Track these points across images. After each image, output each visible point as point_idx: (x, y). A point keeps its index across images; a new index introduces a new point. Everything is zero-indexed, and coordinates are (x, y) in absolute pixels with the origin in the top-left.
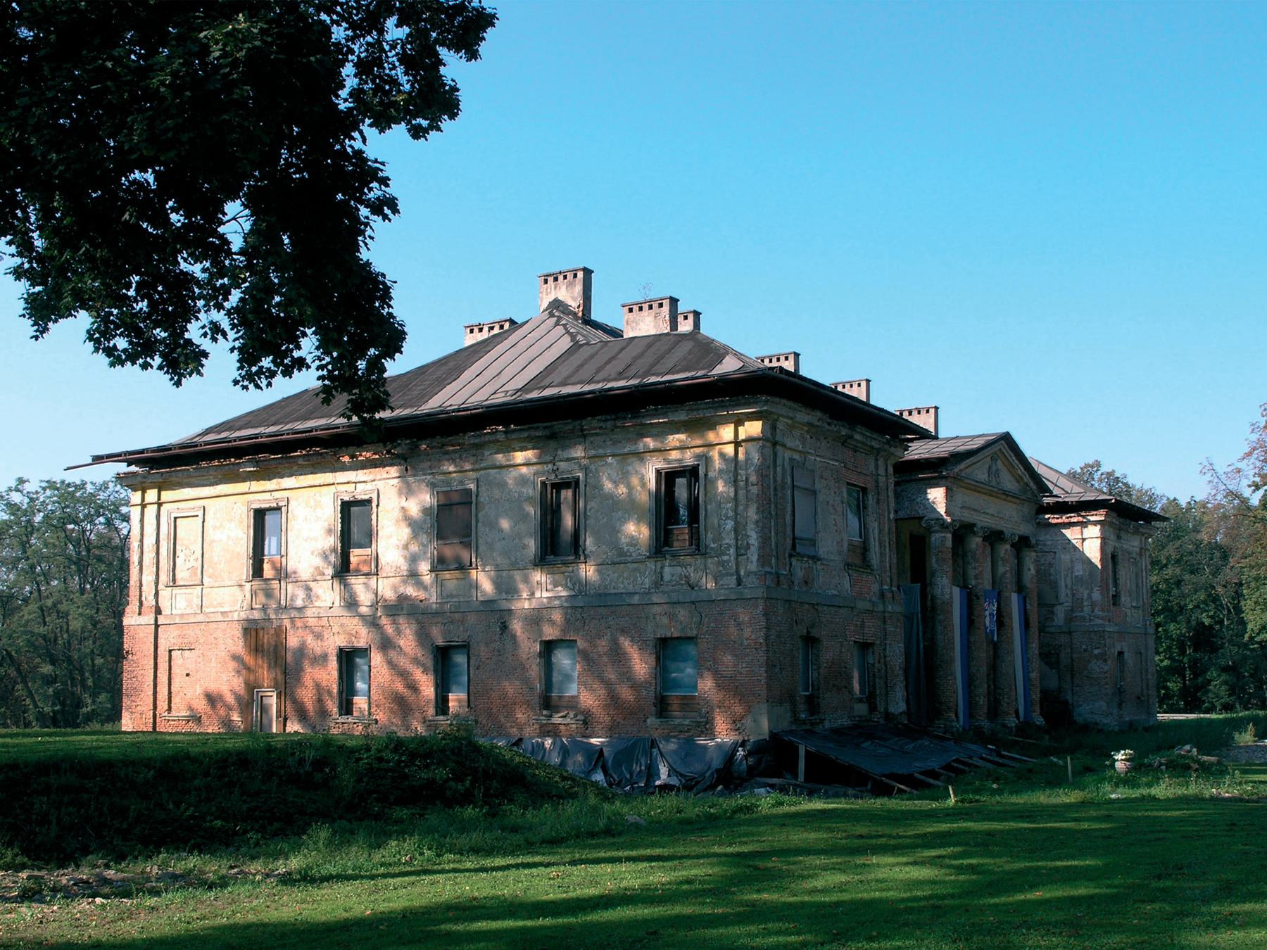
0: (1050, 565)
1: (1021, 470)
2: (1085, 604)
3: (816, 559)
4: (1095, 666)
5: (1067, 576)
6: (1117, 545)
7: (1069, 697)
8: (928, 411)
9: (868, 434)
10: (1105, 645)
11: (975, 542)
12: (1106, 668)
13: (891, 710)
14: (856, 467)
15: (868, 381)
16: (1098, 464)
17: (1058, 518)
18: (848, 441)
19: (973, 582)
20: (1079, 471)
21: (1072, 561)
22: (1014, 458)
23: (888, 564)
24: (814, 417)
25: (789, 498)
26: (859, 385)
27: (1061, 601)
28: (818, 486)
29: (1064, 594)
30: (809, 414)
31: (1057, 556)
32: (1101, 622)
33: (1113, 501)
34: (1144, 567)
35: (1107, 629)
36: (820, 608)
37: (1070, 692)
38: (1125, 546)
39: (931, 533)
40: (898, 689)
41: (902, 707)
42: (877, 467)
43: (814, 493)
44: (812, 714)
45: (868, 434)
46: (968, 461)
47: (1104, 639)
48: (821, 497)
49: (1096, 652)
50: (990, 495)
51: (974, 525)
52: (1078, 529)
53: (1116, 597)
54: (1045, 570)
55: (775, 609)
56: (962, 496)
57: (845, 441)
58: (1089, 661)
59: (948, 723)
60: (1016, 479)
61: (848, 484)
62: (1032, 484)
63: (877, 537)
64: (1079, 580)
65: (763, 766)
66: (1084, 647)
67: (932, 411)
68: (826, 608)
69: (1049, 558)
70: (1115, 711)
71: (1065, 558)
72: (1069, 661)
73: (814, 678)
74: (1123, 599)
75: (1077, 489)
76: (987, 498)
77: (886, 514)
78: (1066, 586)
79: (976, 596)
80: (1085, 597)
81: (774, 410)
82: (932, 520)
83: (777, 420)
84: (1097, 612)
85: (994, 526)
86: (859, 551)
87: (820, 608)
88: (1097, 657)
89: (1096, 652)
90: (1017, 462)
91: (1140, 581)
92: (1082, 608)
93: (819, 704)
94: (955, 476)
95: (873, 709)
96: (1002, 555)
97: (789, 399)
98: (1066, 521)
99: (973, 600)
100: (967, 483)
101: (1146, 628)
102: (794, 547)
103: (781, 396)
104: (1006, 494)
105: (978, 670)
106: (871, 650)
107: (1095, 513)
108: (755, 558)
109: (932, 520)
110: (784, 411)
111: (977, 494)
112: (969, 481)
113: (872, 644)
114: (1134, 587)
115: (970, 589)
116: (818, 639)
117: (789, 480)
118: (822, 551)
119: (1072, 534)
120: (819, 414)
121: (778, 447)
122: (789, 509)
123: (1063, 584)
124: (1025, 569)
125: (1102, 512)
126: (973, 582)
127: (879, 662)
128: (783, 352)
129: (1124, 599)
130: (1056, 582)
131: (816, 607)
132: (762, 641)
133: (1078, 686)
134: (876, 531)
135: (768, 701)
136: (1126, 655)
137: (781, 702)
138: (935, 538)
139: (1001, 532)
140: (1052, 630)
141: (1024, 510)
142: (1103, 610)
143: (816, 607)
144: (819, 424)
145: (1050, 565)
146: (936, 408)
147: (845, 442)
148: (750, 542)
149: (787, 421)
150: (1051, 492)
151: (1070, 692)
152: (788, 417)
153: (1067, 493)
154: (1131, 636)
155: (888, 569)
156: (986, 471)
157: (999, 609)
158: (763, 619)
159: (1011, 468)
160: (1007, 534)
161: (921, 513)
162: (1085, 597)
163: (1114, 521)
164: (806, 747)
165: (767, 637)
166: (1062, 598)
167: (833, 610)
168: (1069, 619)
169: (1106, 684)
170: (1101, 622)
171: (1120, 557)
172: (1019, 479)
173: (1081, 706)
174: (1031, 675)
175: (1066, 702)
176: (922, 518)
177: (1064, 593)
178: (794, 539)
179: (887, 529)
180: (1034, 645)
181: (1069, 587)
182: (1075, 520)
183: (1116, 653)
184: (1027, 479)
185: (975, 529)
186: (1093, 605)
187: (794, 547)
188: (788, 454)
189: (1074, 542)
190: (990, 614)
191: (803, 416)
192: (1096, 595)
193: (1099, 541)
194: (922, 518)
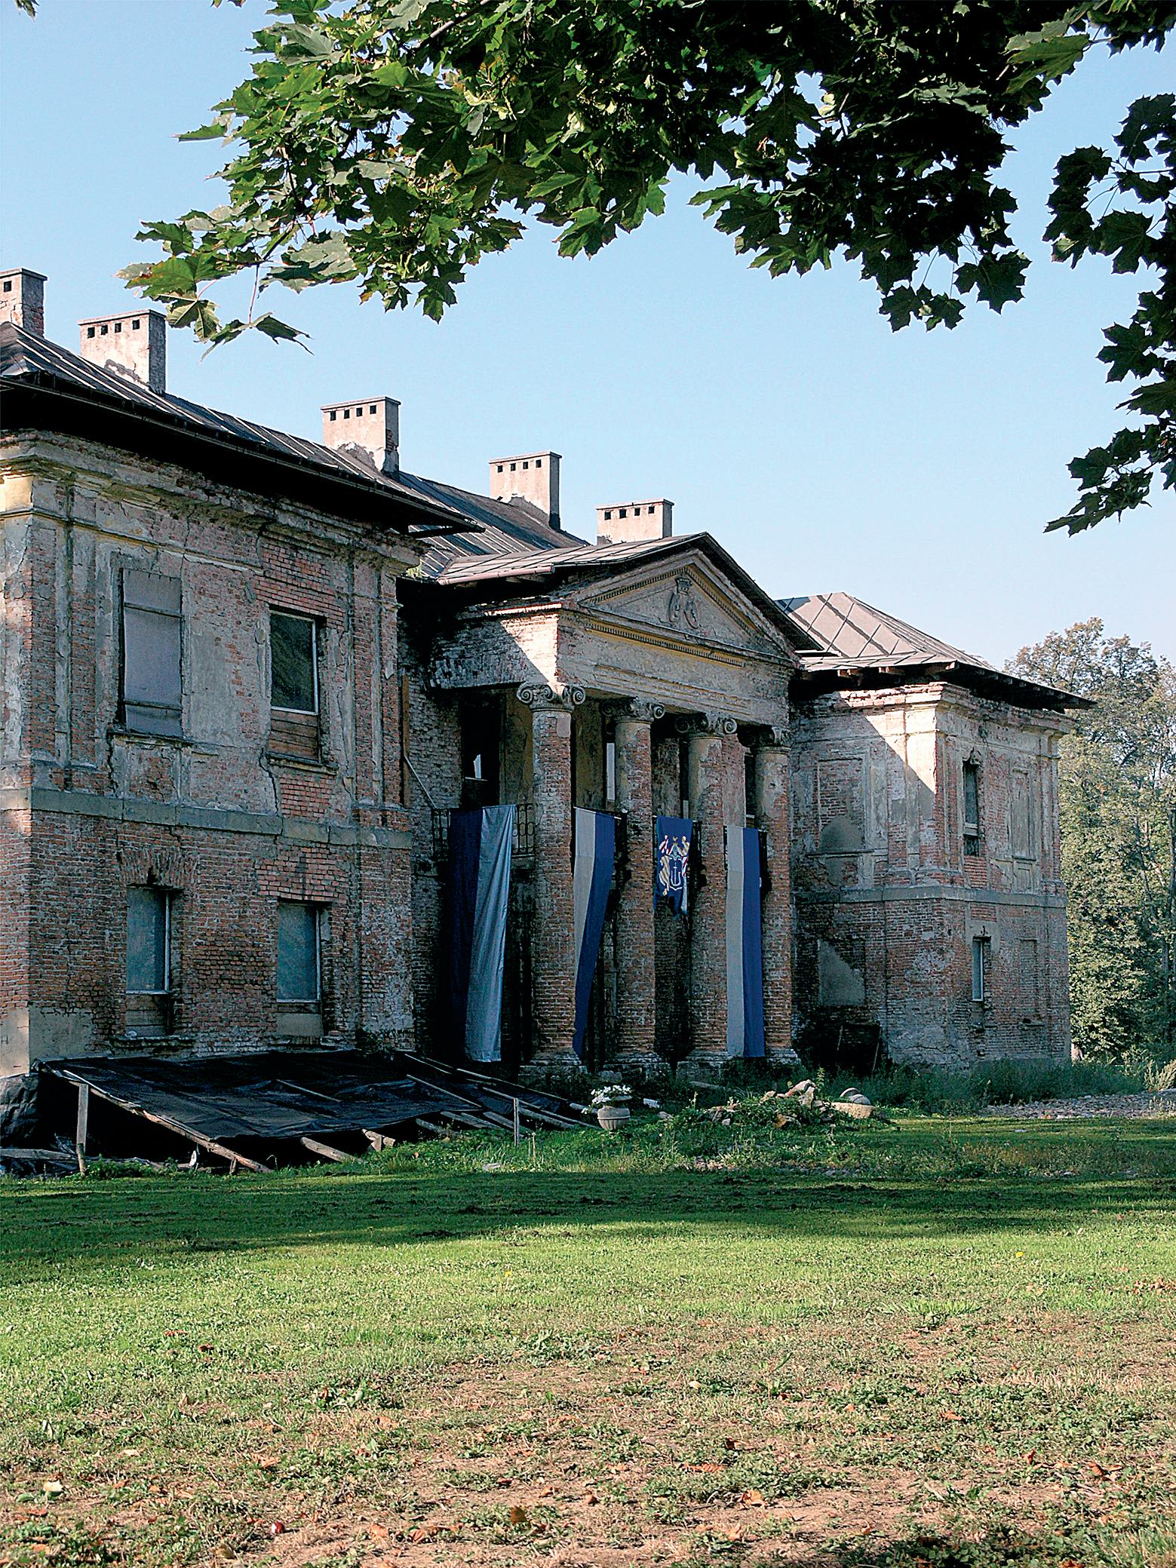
0: (853, 782)
1: (745, 605)
2: (909, 851)
3: (179, 742)
4: (926, 963)
5: (880, 801)
6: (979, 747)
7: (881, 1019)
8: (652, 510)
9: (314, 516)
10: (941, 924)
11: (636, 732)
12: (942, 966)
13: (372, 1027)
14: (295, 578)
15: (555, 458)
16: (1097, 626)
17: (863, 698)
18: (272, 528)
19: (630, 804)
20: (1065, 637)
21: (887, 775)
22: (728, 582)
23: (376, 759)
24: (168, 476)
25: (111, 628)
26: (539, 464)
27: (870, 847)
28: (189, 608)
29: (874, 835)
30: (150, 470)
31: (864, 763)
32: (936, 883)
33: (952, 666)
34: (1045, 790)
35: (944, 895)
36: (184, 834)
37: (882, 1009)
38: (999, 751)
39: (532, 711)
40: (390, 989)
41: (403, 1020)
42: (351, 580)
43: (180, 620)
44: (170, 1031)
45: (314, 516)
46: (609, 581)
47: (940, 914)
48: (196, 628)
49: (927, 936)
50: (668, 647)
51: (629, 700)
52: (898, 714)
53: (973, 843)
54: (843, 792)
55: (57, 832)
56: (594, 646)
57: (264, 526)
58: (914, 953)
59: (557, 1057)
60: (738, 621)
61: (272, 607)
62: (772, 630)
63: (348, 707)
64: (899, 809)
65: (13, 1125)
66: (906, 927)
67: (659, 509)
68: (202, 834)
69: (850, 769)
70: (963, 1044)
71: (878, 768)
72: (882, 952)
73: (174, 965)
74: (992, 844)
75: (903, 647)
76: (663, 651)
77: (376, 667)
78: (878, 818)
79: (635, 828)
80: (909, 838)
81: (57, 459)
82: (532, 688)
83: (71, 478)
84: (929, 865)
85: (679, 703)
86: (304, 731)
87: (184, 834)
88: (927, 946)
89: (927, 936)
90: (734, 589)
91: (1037, 815)
92: (904, 858)
93: (180, 1012)
94: (576, 607)
95: (328, 1026)
96: (704, 757)
97: (91, 438)
98: (878, 703)
99: (627, 836)
100: (604, 622)
101: (1046, 898)
102: (120, 717)
103: (71, 431)
104: (709, 648)
105: (636, 963)
106: (326, 915)
107: (924, 687)
108: (16, 736)
109: (532, 688)
110: (81, 462)
111: (638, 645)
112: (608, 619)
113: (326, 905)
114: (1021, 824)
115: (624, 816)
116: (181, 891)
117: (111, 592)
118: (198, 725)
119: (884, 725)
120: (176, 471)
121: (75, 529)
122: (110, 646)
123: (874, 816)
124: (766, 784)
125: (937, 686)
126: (630, 804)
127: (344, 937)
128: (367, 399)
129: (992, 844)
130: (862, 814)
131: (178, 832)
132: (23, 891)
133: (895, 997)
134: (348, 699)
135: (30, 1003)
136: (995, 945)
137: (66, 1004)
138: (540, 719)
139: (701, 716)
140: (854, 897)
141: (759, 677)
142: (938, 863)
143: (178, 832)
144: (180, 490)
145: (853, 782)
146: (668, 505)
147: (263, 529)
148: (9, 706)
149: (100, 481)
150: (820, 648)
151: (882, 1009)
152: (101, 475)
153: (885, 653)
154: (1009, 909)
155: (378, 768)
156: (662, 604)
157: (695, 858)
158: (26, 850)
159: (724, 603)
160: (712, 719)
161: (516, 675)
162: (909, 838)
163: (965, 702)
164: (90, 1087)
165: (33, 883)
166: (871, 841)
167: (222, 839)
168: (883, 879)
169: (943, 994)
170: (936, 883)
171: (985, 770)
172: (744, 622)
173: (899, 1033)
174: (773, 974)
175: (875, 1029)
176: (518, 684)
177: (873, 831)
178: (121, 703)
179: (375, 696)
180: (780, 922)
181: (883, 821)
182: (891, 701)
183: (970, 940)
184: (760, 620)
185: (633, 707)
186: (922, 853)
187: (120, 717)
188: (106, 546)
189: (889, 741)
190: (672, 863)
191: (133, 472)
192: (928, 836)
193: (933, 737)
194: (518, 684)
